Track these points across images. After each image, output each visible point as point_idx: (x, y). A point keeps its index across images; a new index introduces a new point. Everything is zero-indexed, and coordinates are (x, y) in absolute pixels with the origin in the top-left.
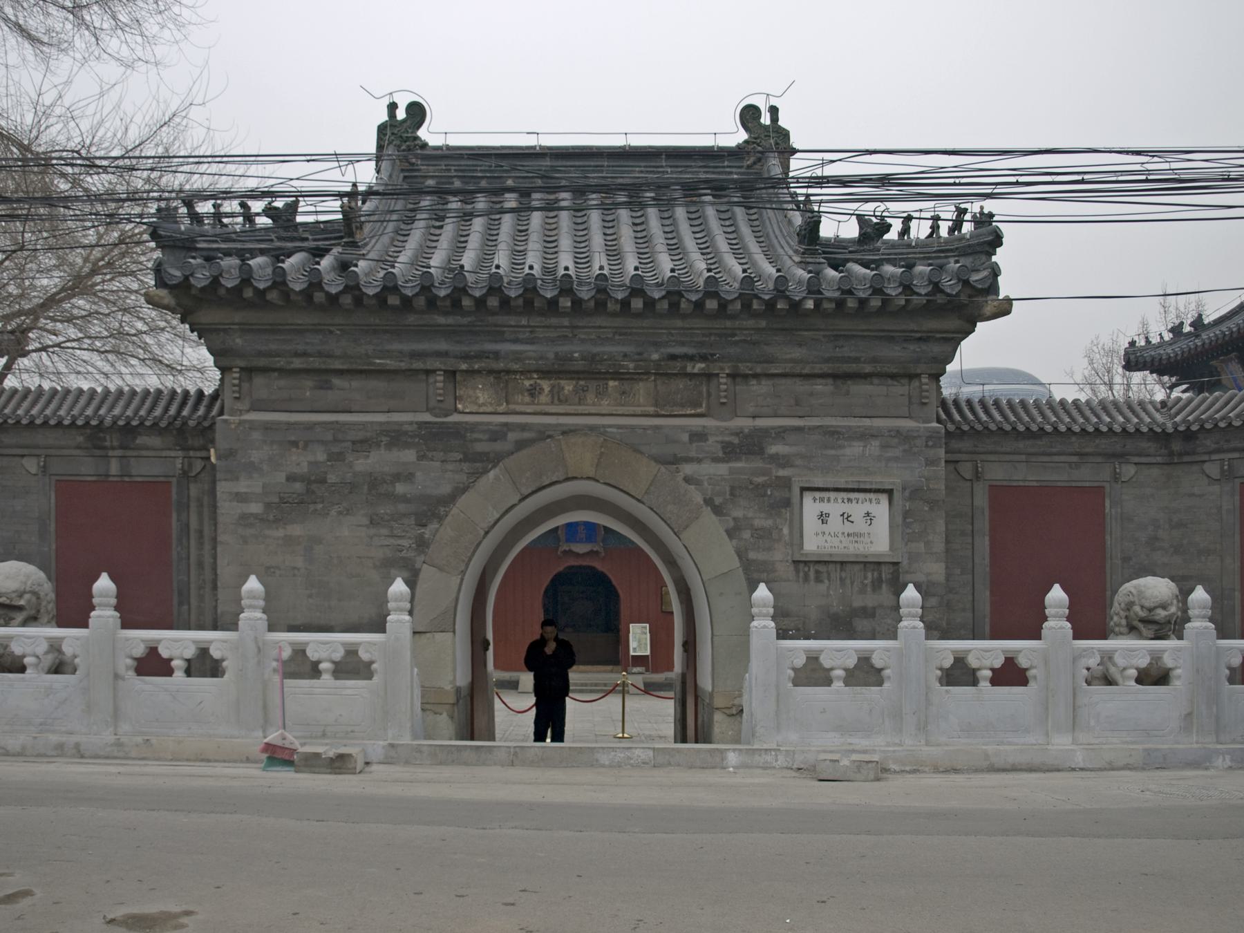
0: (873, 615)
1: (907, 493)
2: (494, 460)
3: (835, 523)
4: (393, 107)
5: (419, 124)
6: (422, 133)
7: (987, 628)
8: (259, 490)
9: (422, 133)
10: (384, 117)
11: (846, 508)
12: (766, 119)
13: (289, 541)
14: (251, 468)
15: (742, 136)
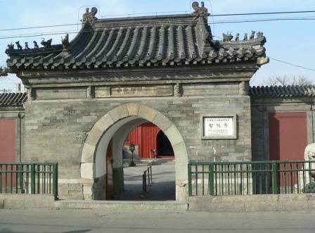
0: (228, 155)
1: (195, 119)
2: (105, 112)
3: (215, 127)
6: (96, 16)
7: (269, 157)
8: (36, 122)
9: (96, 16)
10: (85, 12)
11: (218, 122)
12: (200, 6)
13: (45, 137)
14: (34, 116)
15: (194, 11)
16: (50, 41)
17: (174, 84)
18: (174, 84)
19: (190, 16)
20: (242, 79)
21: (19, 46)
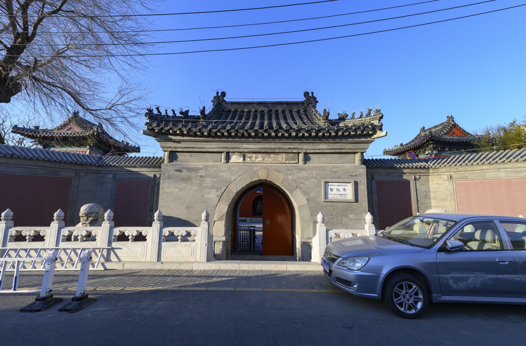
3: (335, 191)
4: (218, 93)
5: (224, 96)
6: (225, 99)
9: (225, 99)
12: (310, 95)
15: (304, 99)
16: (188, 111)
17: (299, 153)
18: (299, 153)
19: (302, 103)
20: (358, 151)
21: (159, 112)
